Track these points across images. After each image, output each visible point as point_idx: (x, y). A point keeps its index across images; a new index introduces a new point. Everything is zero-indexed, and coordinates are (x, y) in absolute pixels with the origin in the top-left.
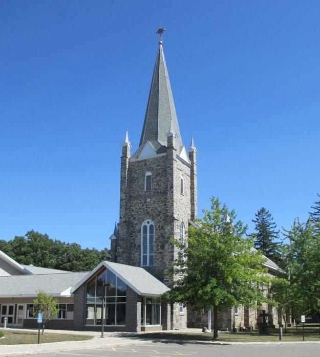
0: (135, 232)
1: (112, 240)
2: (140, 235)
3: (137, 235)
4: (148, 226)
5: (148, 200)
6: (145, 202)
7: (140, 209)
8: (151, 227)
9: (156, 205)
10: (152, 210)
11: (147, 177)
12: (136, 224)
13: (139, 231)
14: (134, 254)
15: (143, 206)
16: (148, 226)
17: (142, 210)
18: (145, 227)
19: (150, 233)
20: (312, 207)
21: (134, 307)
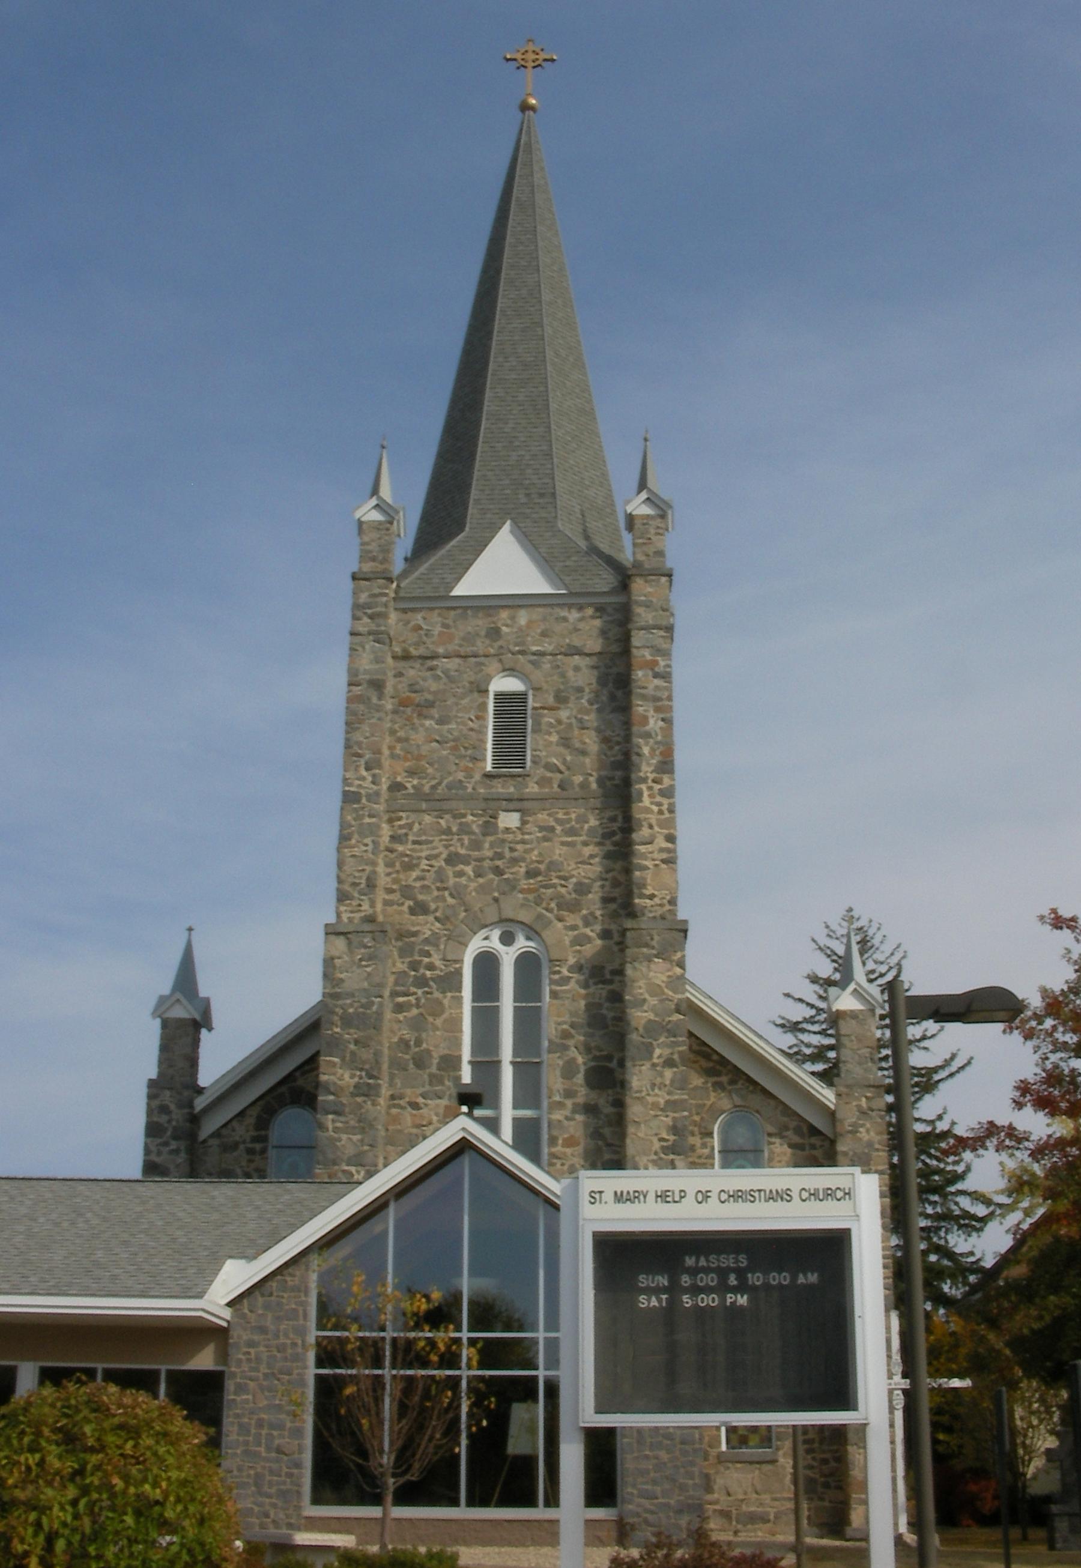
0: (422, 982)
1: (165, 1024)
2: (459, 1000)
3: (440, 1003)
4: (508, 957)
5: (509, 820)
6: (489, 827)
7: (452, 859)
8: (527, 965)
9: (558, 852)
10: (531, 874)
11: (500, 697)
12: (433, 940)
13: (452, 982)
14: (415, 1106)
15: (476, 845)
16: (508, 957)
17: (469, 870)
18: (487, 965)
19: (477, 996)
20: (788, 995)
21: (164, 1109)
